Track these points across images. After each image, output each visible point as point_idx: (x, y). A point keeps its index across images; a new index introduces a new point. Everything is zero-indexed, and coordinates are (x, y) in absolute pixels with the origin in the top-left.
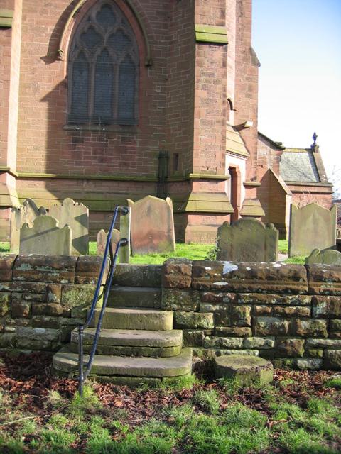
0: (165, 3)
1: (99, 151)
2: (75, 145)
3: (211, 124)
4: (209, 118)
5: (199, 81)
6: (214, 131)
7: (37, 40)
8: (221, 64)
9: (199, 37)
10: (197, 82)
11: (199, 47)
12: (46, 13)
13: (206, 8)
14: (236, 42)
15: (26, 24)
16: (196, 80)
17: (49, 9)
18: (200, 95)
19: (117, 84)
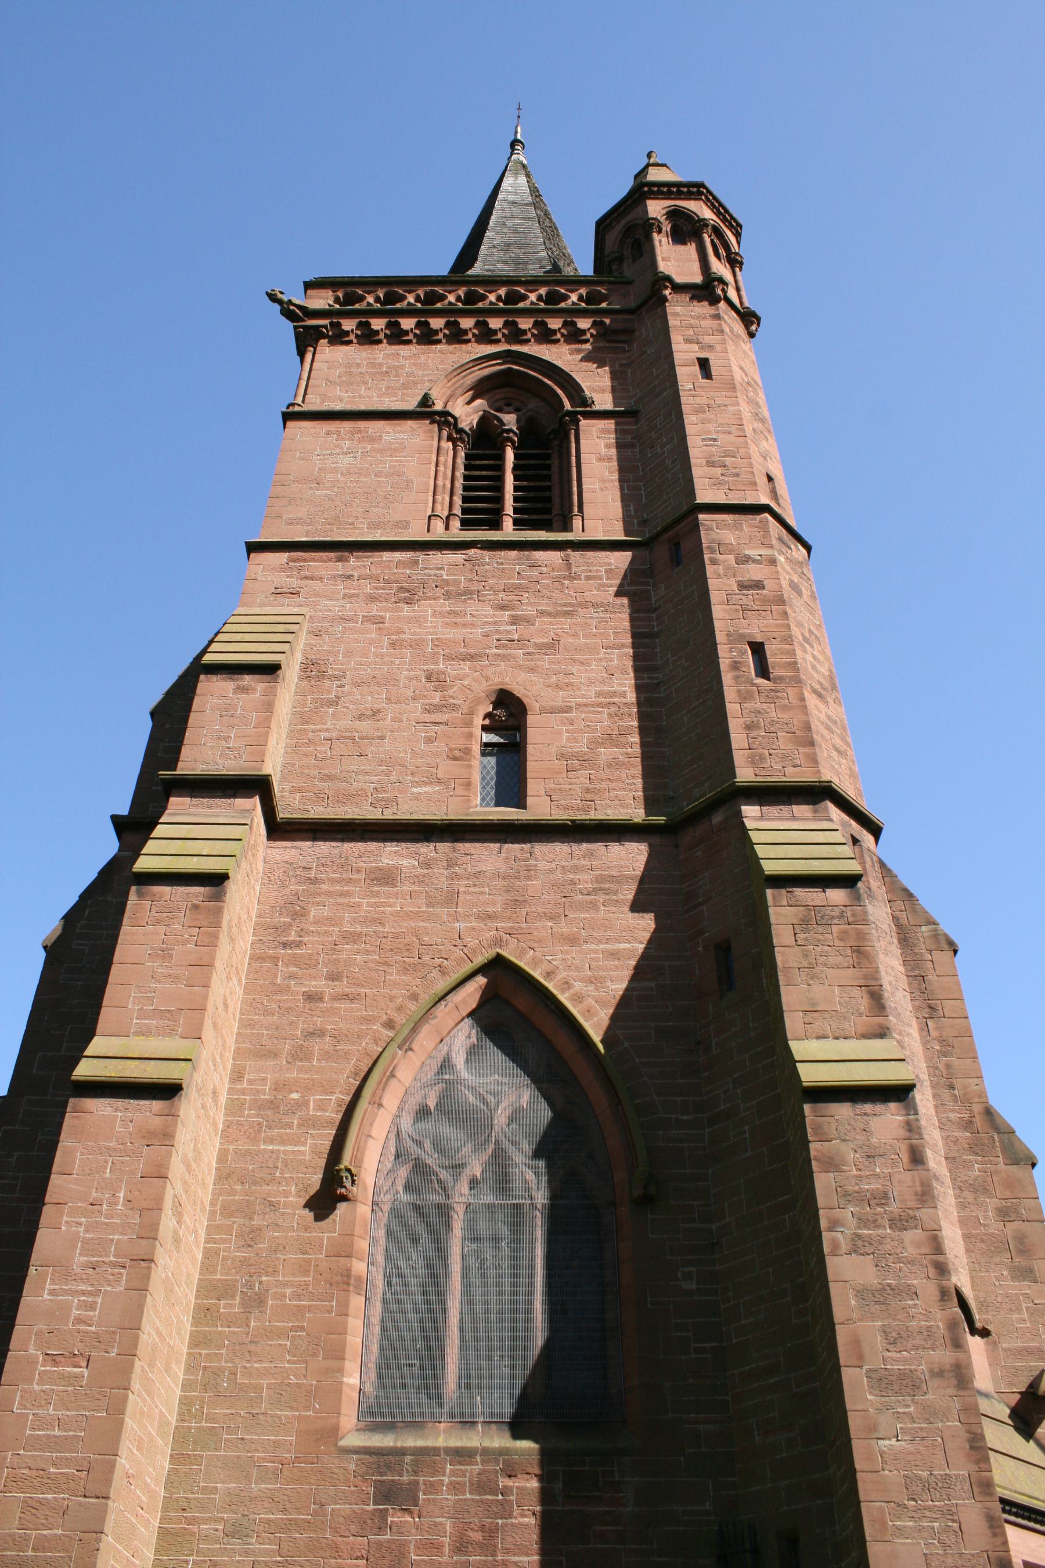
0: (648, 695)
1: (477, 1536)
2: (384, 1514)
3: (909, 1384)
4: (897, 1361)
5: (834, 1224)
6: (930, 1413)
7: (271, 1140)
8: (905, 1157)
9: (810, 1075)
10: (830, 1229)
11: (814, 1111)
12: (307, 1056)
13: (818, 991)
14: (935, 1096)
15: (243, 1092)
16: (823, 1223)
17: (317, 1046)
18: (848, 1274)
19: (271, 1147)
